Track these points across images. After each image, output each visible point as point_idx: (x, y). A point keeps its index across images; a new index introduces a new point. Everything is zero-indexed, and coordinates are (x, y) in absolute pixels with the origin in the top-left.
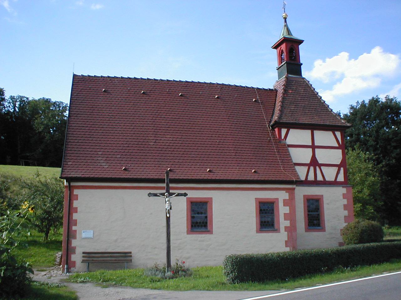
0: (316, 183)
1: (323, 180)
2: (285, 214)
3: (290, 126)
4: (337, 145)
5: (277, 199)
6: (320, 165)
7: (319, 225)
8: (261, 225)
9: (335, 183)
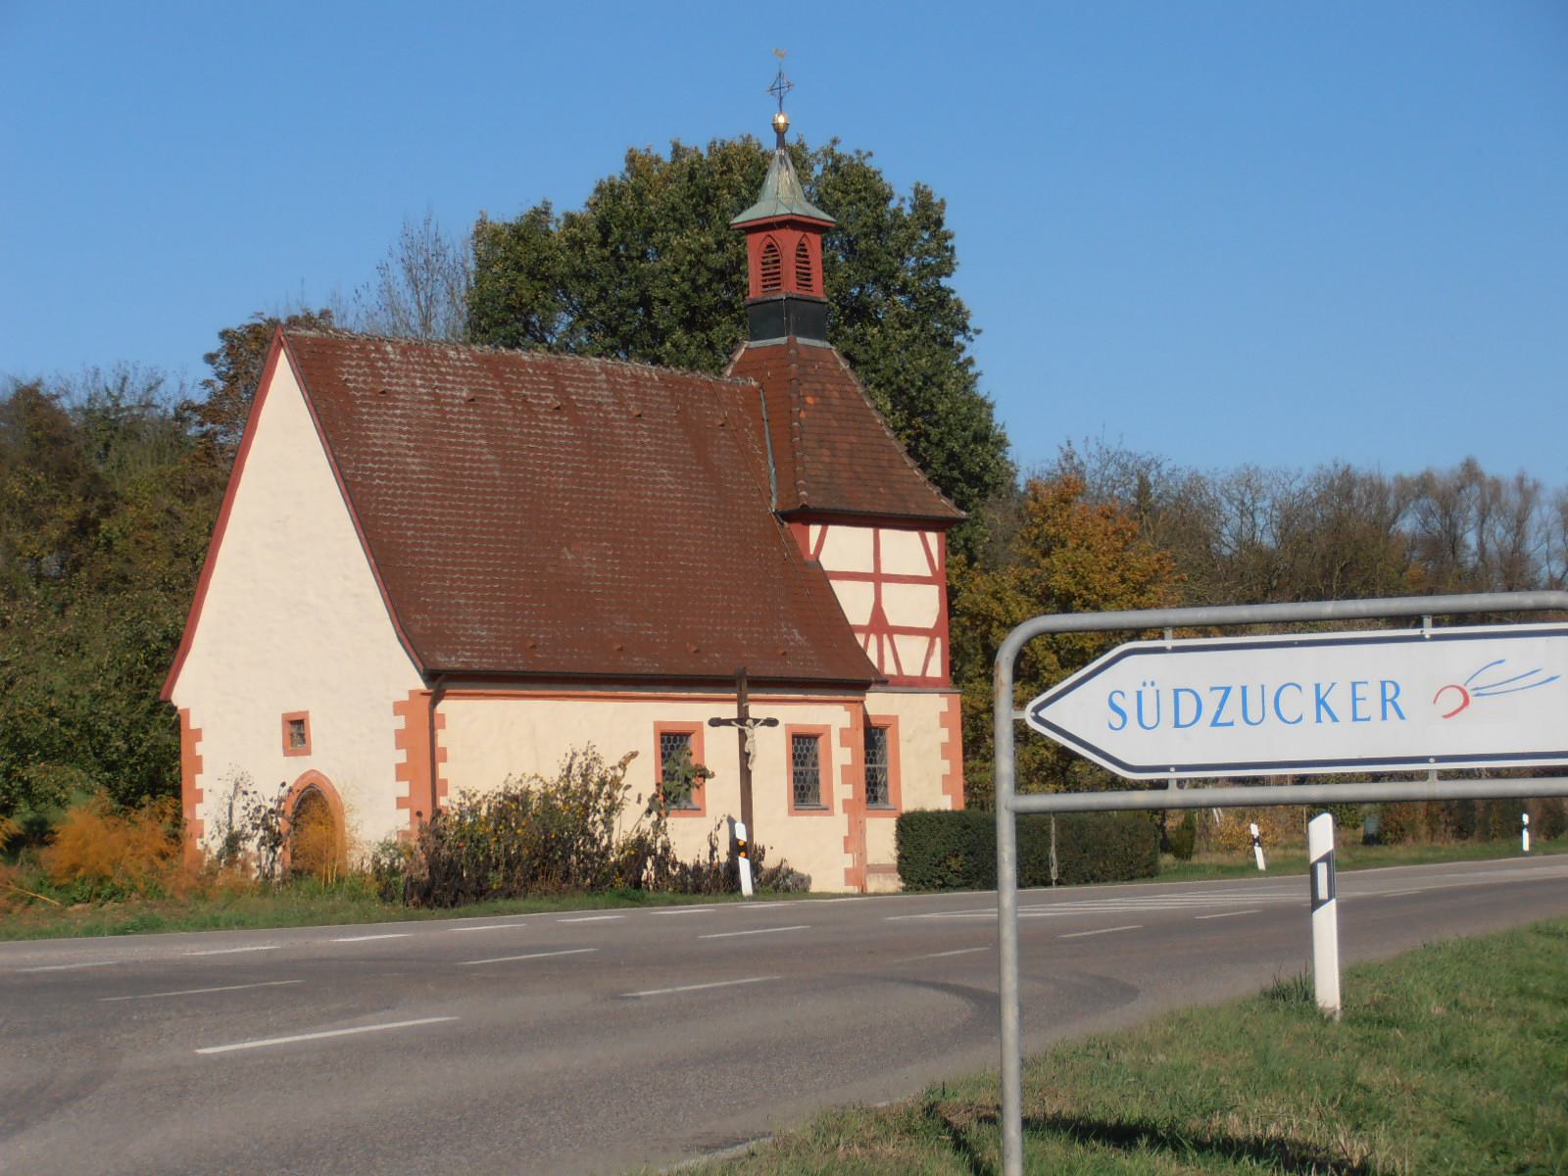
2: (843, 766)
3: (828, 518)
4: (927, 573)
5: (828, 727)
7: (662, 734)
8: (663, 755)
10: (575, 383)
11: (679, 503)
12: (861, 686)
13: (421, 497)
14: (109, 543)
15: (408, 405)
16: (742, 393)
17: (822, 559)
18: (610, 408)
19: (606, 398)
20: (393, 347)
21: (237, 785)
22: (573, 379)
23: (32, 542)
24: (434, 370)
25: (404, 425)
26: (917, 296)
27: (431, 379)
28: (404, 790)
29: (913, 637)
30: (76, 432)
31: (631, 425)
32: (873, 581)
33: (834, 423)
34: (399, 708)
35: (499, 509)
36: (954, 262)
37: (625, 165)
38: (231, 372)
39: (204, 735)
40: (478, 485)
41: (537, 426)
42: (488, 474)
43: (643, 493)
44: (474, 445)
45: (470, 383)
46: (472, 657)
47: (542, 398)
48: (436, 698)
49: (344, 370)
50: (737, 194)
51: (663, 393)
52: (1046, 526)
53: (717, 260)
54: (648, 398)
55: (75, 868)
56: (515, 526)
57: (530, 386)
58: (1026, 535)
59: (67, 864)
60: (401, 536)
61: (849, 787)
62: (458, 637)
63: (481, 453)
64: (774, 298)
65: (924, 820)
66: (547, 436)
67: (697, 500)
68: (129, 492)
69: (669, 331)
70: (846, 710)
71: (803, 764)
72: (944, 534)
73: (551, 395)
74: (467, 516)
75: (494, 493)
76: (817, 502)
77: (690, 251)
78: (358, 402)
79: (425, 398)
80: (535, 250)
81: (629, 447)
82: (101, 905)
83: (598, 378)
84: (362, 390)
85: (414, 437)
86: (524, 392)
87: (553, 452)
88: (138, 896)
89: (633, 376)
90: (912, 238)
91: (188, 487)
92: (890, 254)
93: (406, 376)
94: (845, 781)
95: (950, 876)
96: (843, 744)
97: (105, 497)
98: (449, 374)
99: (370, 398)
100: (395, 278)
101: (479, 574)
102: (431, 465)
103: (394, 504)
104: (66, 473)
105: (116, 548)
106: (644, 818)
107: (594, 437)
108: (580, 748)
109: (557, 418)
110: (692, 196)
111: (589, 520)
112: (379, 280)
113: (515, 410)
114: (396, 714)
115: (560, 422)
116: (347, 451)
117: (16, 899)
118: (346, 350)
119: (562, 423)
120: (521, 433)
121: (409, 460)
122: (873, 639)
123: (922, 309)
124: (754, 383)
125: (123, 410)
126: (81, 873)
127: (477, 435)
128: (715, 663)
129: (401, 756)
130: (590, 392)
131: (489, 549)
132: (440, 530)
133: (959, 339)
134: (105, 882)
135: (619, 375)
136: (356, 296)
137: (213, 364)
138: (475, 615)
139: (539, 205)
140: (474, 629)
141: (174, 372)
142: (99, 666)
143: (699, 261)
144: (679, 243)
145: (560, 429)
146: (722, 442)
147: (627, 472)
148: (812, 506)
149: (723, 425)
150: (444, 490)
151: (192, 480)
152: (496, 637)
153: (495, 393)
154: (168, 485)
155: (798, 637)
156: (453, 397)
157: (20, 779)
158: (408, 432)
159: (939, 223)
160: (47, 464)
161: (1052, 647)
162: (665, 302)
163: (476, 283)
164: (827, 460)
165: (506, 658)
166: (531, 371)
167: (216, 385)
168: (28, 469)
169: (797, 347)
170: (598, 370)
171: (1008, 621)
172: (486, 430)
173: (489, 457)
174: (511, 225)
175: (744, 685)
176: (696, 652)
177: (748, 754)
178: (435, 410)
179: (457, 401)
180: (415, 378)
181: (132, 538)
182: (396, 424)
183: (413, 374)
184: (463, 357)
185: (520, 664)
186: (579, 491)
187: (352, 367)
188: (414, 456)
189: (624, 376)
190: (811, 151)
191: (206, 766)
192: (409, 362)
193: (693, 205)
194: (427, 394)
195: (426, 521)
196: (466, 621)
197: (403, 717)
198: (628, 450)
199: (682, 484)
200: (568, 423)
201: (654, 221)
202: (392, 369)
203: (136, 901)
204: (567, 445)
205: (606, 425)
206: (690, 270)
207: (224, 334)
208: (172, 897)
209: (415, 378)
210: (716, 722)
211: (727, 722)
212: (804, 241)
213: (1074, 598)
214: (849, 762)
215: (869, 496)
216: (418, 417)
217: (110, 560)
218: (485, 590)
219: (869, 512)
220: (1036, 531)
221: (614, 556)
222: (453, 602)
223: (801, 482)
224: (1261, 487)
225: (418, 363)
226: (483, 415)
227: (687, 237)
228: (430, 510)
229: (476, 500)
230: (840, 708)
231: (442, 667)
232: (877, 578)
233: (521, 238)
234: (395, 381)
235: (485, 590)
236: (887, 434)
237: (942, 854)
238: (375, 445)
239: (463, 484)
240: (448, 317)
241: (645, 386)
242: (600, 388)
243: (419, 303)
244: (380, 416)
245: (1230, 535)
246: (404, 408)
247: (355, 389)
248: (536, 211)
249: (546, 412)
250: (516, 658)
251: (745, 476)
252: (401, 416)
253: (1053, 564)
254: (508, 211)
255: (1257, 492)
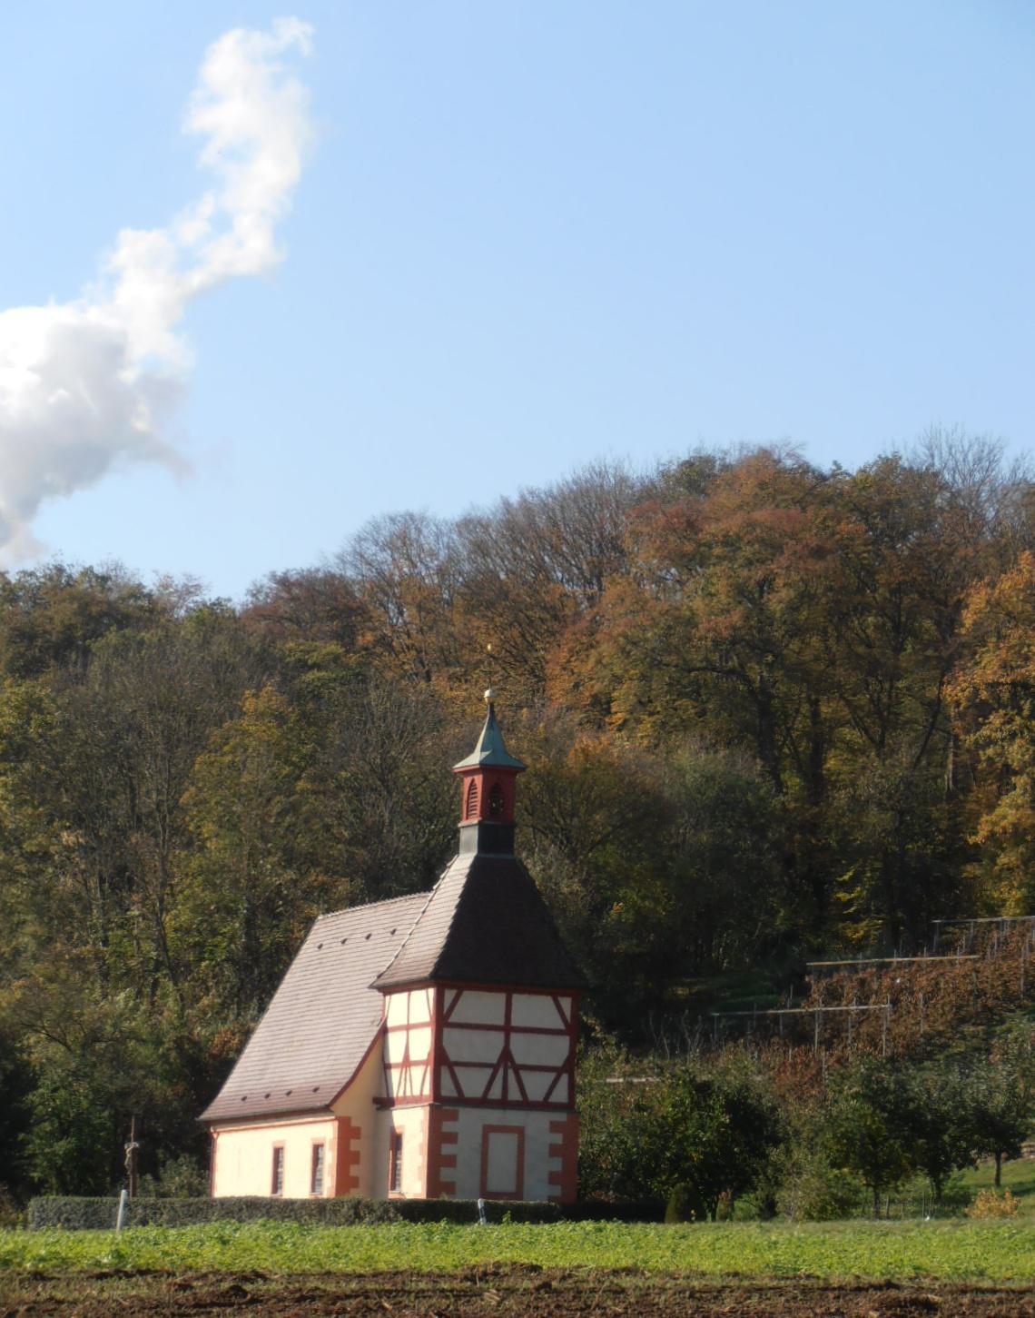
0: (504, 1104)
1: (521, 1099)
4: (561, 1026)
6: (518, 1069)
9: (545, 1105)
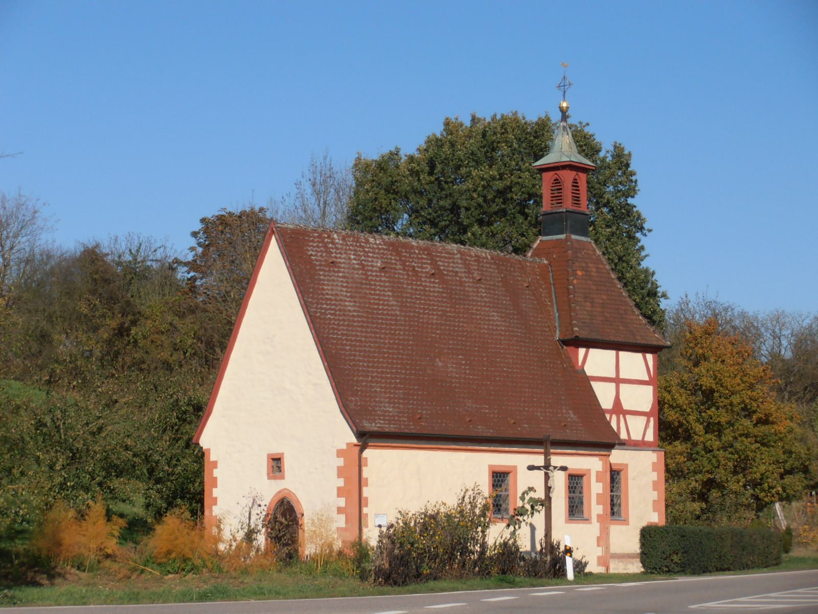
3: (590, 344)
4: (646, 378)
5: (589, 470)
7: (493, 472)
8: (493, 485)
10: (442, 260)
11: (503, 333)
12: (609, 446)
13: (353, 326)
14: (136, 342)
15: (346, 271)
16: (538, 267)
17: (586, 368)
18: (463, 275)
19: (460, 269)
20: (338, 235)
21: (254, 500)
22: (441, 257)
23: (91, 339)
24: (362, 250)
25: (344, 283)
26: (615, 209)
27: (359, 255)
28: (342, 502)
29: (638, 417)
30: (119, 276)
31: (475, 285)
32: (615, 382)
33: (594, 287)
34: (340, 453)
35: (399, 334)
36: (637, 189)
37: (442, 127)
38: (207, 243)
39: (219, 465)
40: (387, 319)
41: (421, 285)
42: (393, 312)
43: (482, 326)
44: (384, 296)
45: (382, 258)
46: (384, 423)
47: (424, 268)
48: (363, 448)
49: (309, 249)
50: (510, 147)
51: (493, 266)
52: (696, 349)
53: (499, 185)
54: (485, 269)
55: (169, 552)
56: (408, 345)
57: (416, 261)
58: (684, 353)
59: (164, 550)
60: (342, 350)
61: (601, 507)
62: (375, 411)
63: (388, 301)
64: (558, 211)
65: (657, 531)
66: (426, 291)
67: (513, 331)
68: (148, 312)
69: (470, 225)
70: (600, 460)
71: (574, 492)
72: (656, 355)
73: (429, 266)
74: (380, 338)
75: (396, 325)
76: (584, 334)
77: (483, 179)
78: (318, 268)
79: (356, 266)
80: (390, 176)
81: (474, 298)
82: (185, 576)
83: (456, 256)
84: (320, 261)
85: (350, 290)
86: (413, 264)
87: (430, 301)
88: (207, 570)
89: (476, 256)
90: (613, 174)
91: (182, 310)
92: (600, 183)
93: (345, 253)
94: (598, 503)
95: (673, 565)
96: (597, 481)
97: (134, 315)
98: (369, 252)
99: (325, 266)
100: (305, 190)
101: (388, 373)
102: (359, 307)
103: (339, 330)
104: (112, 299)
105: (140, 345)
106: (505, 529)
107: (453, 292)
108: (470, 486)
109: (432, 280)
110: (484, 147)
111: (451, 342)
112: (296, 191)
113: (408, 275)
114: (338, 456)
115: (434, 282)
116: (312, 298)
117: (134, 570)
118: (310, 237)
119: (436, 283)
120: (412, 289)
121: (347, 304)
122: (614, 417)
123: (617, 216)
124: (545, 262)
125: (139, 263)
126: (173, 555)
127: (386, 289)
128: (525, 431)
129: (341, 483)
130: (451, 265)
131: (394, 359)
132: (365, 346)
133: (638, 235)
134: (187, 561)
135: (468, 255)
136: (282, 200)
137: (196, 238)
138: (386, 398)
139: (393, 150)
140: (385, 407)
141: (161, 239)
142: (153, 420)
143: (488, 185)
144: (476, 174)
145: (434, 287)
146: (528, 297)
147: (473, 314)
148: (581, 337)
149: (528, 287)
150: (368, 322)
151: (185, 306)
152: (397, 412)
153: (396, 264)
154: (171, 308)
155: (572, 415)
156: (372, 266)
157: (109, 488)
158: (347, 287)
159: (628, 165)
160: (100, 294)
161: (699, 420)
162: (467, 209)
163: (355, 194)
164: (588, 309)
165: (404, 425)
166: (417, 251)
167: (197, 250)
168: (90, 297)
169: (571, 240)
170: (456, 252)
171: (674, 405)
172: (393, 287)
173: (393, 303)
174: (376, 161)
175: (549, 444)
176: (514, 423)
177: (550, 488)
178: (362, 274)
179: (375, 269)
180: (351, 254)
181: (149, 339)
182: (340, 282)
183: (349, 252)
184: (378, 242)
185: (412, 429)
186: (446, 325)
187: (314, 247)
188: (350, 301)
189: (471, 256)
190: (553, 121)
191: (219, 483)
192: (347, 245)
193: (485, 152)
194: (358, 264)
195: (357, 341)
196: (381, 402)
197: (342, 459)
198: (473, 300)
199: (505, 321)
200: (438, 283)
201: (461, 161)
202: (337, 249)
203: (205, 573)
204: (437, 296)
205: (461, 285)
206: (483, 190)
207: (203, 220)
208: (227, 572)
209: (351, 254)
210: (531, 468)
211: (538, 468)
212: (577, 177)
213: (714, 392)
214: (601, 491)
215: (614, 331)
216: (352, 278)
217: (136, 352)
218: (391, 383)
219: (614, 341)
220: (691, 351)
221: (466, 365)
222: (373, 390)
223: (575, 322)
224: (785, 323)
225: (351, 245)
226: (390, 277)
227: (481, 170)
228: (359, 334)
229: (385, 329)
230: (596, 459)
231: (367, 429)
232: (618, 381)
233: (382, 169)
234: (339, 256)
235: (391, 383)
236: (624, 294)
237: (668, 553)
238: (327, 294)
239: (378, 319)
240: (336, 215)
241: (483, 262)
242: (457, 263)
243: (319, 205)
244: (330, 276)
245: (767, 350)
246: (343, 272)
247: (316, 260)
248: (391, 153)
249: (426, 277)
250: (409, 425)
251: (541, 318)
252: (343, 277)
253: (701, 371)
254: (373, 154)
255: (783, 325)
